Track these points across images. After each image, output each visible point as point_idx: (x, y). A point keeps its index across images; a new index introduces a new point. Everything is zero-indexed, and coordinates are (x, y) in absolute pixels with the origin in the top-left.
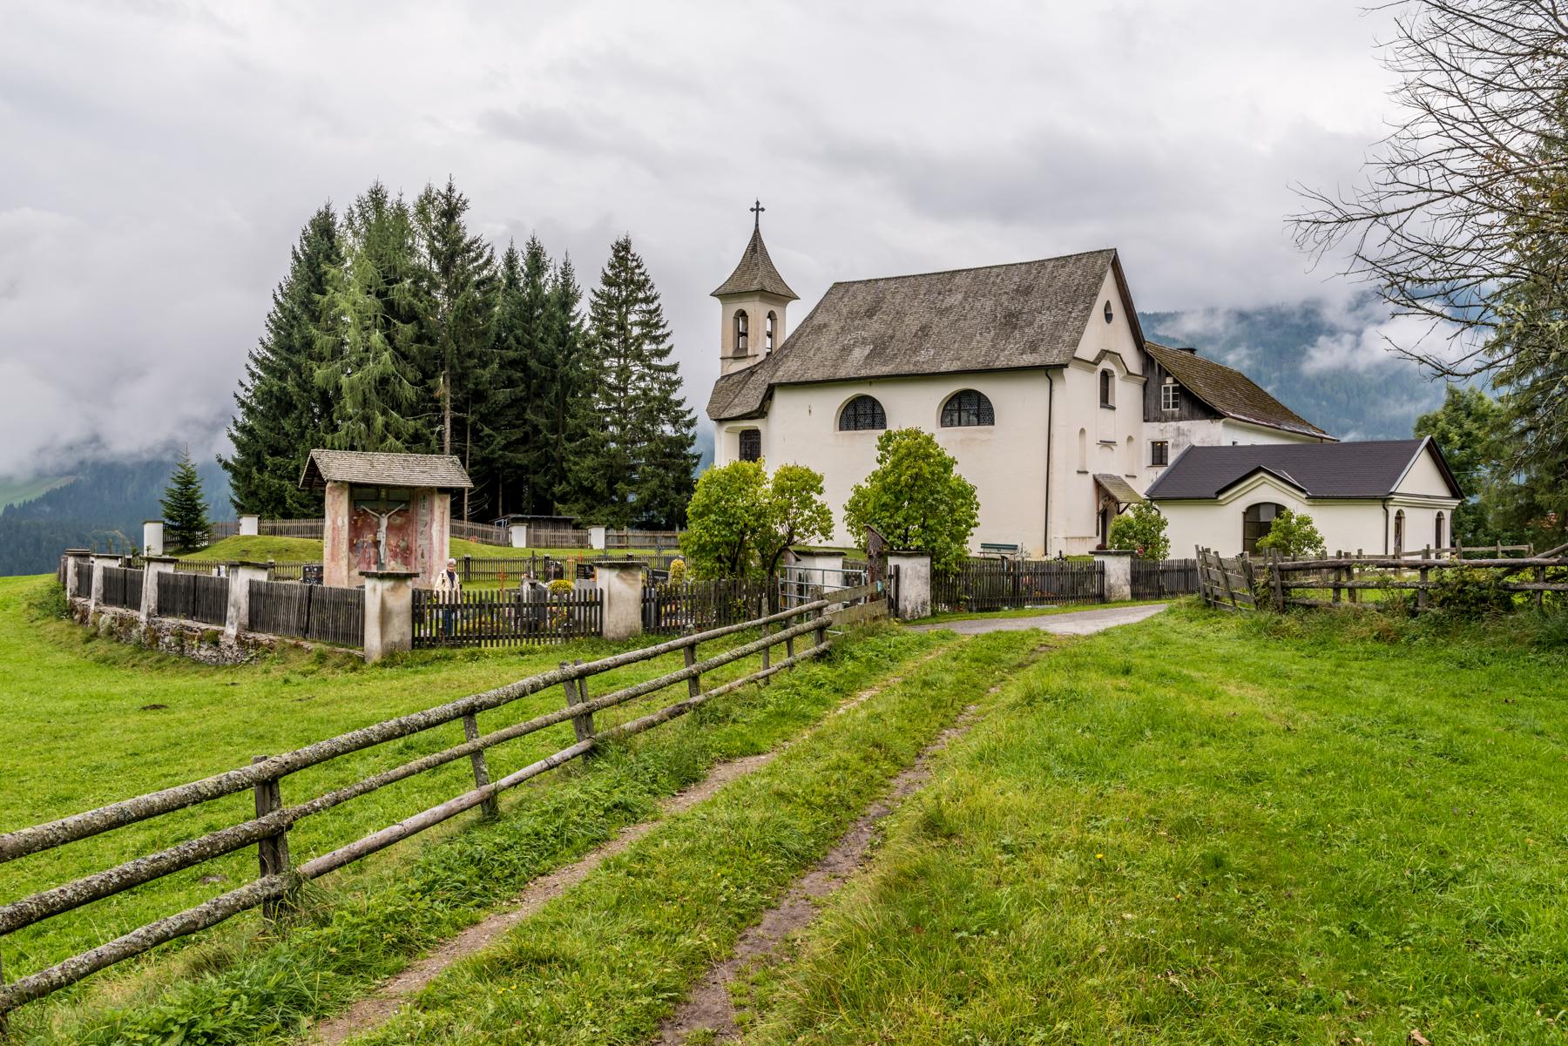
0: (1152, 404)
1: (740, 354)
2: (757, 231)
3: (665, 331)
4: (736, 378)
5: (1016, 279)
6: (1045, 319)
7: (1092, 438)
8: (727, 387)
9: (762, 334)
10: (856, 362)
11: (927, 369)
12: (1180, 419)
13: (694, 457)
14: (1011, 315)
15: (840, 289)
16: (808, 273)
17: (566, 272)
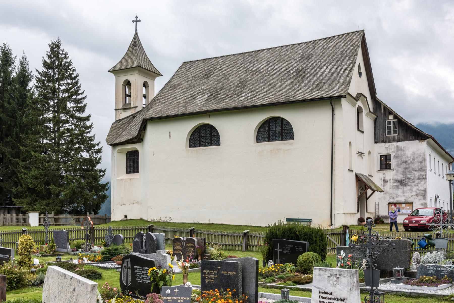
0: (380, 133)
1: (126, 108)
2: (136, 34)
3: (83, 96)
4: (124, 121)
5: (300, 51)
6: (324, 71)
7: (355, 149)
8: (118, 125)
9: (140, 96)
11: (248, 104)
12: (399, 140)
13: (100, 171)
14: (300, 70)
17: (23, 64)
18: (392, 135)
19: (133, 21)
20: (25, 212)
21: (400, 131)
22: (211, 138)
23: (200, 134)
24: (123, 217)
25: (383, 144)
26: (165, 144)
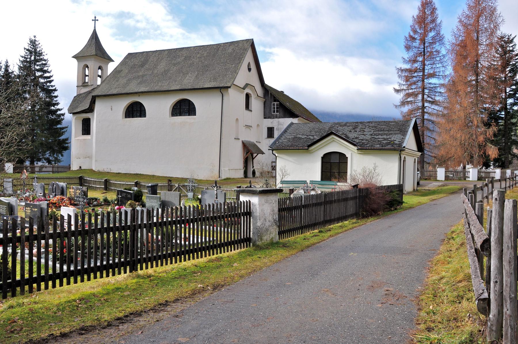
8: (77, 99)
10: (133, 87)
12: (280, 118)
15: (130, 56)
16: (117, 50)
18: (276, 113)
19: (93, 20)
20: (118, 326)
21: (281, 111)
22: (141, 112)
23: (132, 108)
24: (78, 168)
25: (269, 119)
26: (108, 115)
